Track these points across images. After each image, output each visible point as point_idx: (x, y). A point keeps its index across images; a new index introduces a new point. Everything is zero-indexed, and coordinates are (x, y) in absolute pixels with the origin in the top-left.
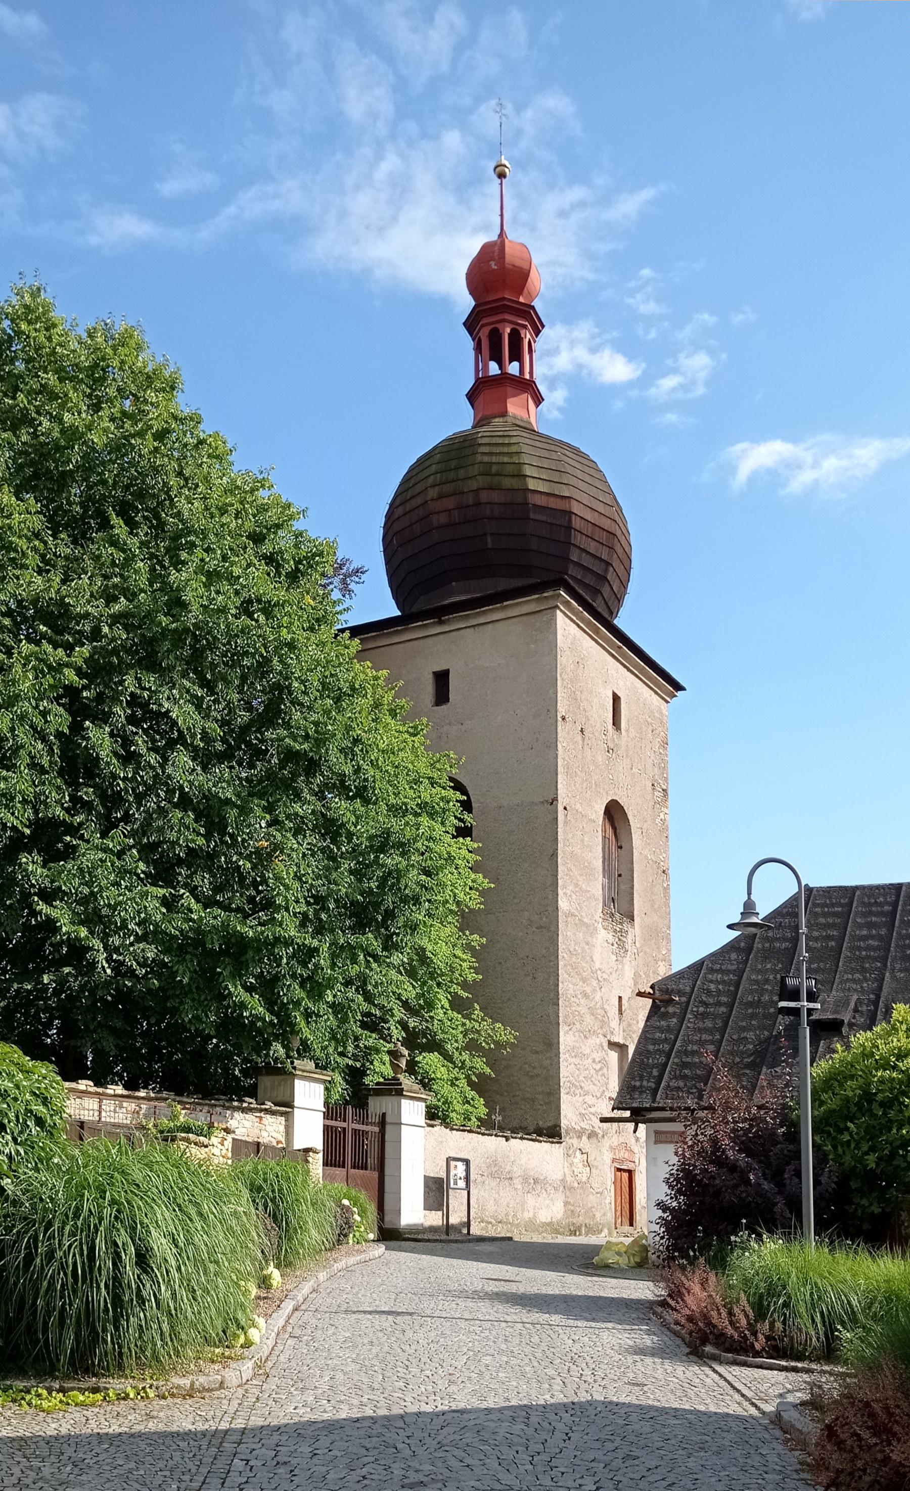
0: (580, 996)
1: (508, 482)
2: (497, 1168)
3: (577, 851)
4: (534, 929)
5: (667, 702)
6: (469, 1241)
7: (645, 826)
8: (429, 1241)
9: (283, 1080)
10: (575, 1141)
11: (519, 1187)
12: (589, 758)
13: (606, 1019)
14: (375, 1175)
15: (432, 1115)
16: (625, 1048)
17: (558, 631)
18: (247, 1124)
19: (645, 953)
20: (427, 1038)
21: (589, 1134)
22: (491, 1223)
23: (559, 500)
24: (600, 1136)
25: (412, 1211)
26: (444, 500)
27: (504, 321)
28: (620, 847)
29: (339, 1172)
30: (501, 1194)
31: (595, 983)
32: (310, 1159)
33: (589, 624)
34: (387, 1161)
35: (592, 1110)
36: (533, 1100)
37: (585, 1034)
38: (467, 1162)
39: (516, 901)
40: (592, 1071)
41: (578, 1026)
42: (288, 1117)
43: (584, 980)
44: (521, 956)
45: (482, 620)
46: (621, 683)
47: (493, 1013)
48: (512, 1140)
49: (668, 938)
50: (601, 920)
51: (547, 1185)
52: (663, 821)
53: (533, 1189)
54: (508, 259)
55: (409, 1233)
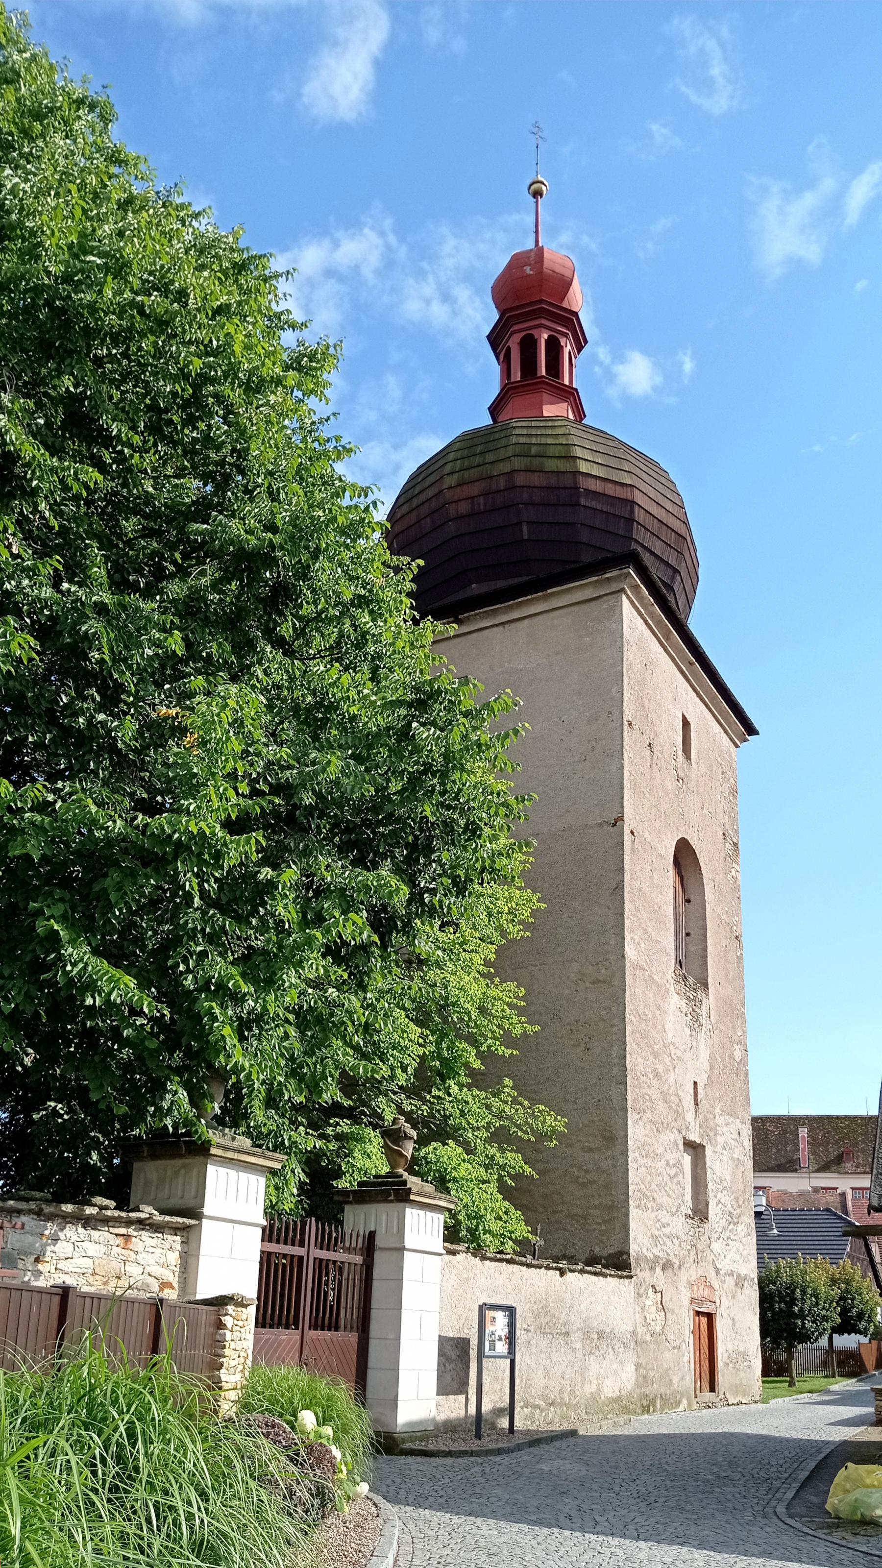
0: (651, 1076)
1: (551, 465)
2: (548, 1319)
3: (645, 888)
4: (588, 984)
5: (737, 746)
6: (519, 1448)
7: (717, 879)
8: (450, 1454)
9: (184, 1166)
10: (647, 1274)
11: (579, 1346)
12: (658, 781)
13: (680, 1109)
14: (353, 1338)
15: (452, 1235)
16: (700, 1150)
17: (624, 618)
18: (92, 1249)
19: (721, 1031)
20: (429, 1128)
21: (664, 1265)
22: (538, 1407)
23: (618, 488)
24: (676, 1266)
25: (418, 1399)
26: (465, 487)
27: (540, 326)
28: (688, 901)
29: (288, 1337)
30: (554, 1359)
31: (667, 1060)
32: (228, 1321)
33: (659, 623)
34: (374, 1314)
35: (666, 1231)
36: (585, 1217)
37: (659, 1128)
38: (511, 1312)
39: (559, 950)
40: (666, 1178)
41: (649, 1115)
42: (189, 1235)
43: (656, 1055)
44: (567, 1021)
45: (515, 615)
46: (691, 709)
47: (528, 1091)
48: (569, 1275)
49: (742, 1017)
50: (673, 982)
51: (615, 1341)
52: (735, 879)
53: (597, 1347)
54: (546, 264)
55: (412, 1440)
